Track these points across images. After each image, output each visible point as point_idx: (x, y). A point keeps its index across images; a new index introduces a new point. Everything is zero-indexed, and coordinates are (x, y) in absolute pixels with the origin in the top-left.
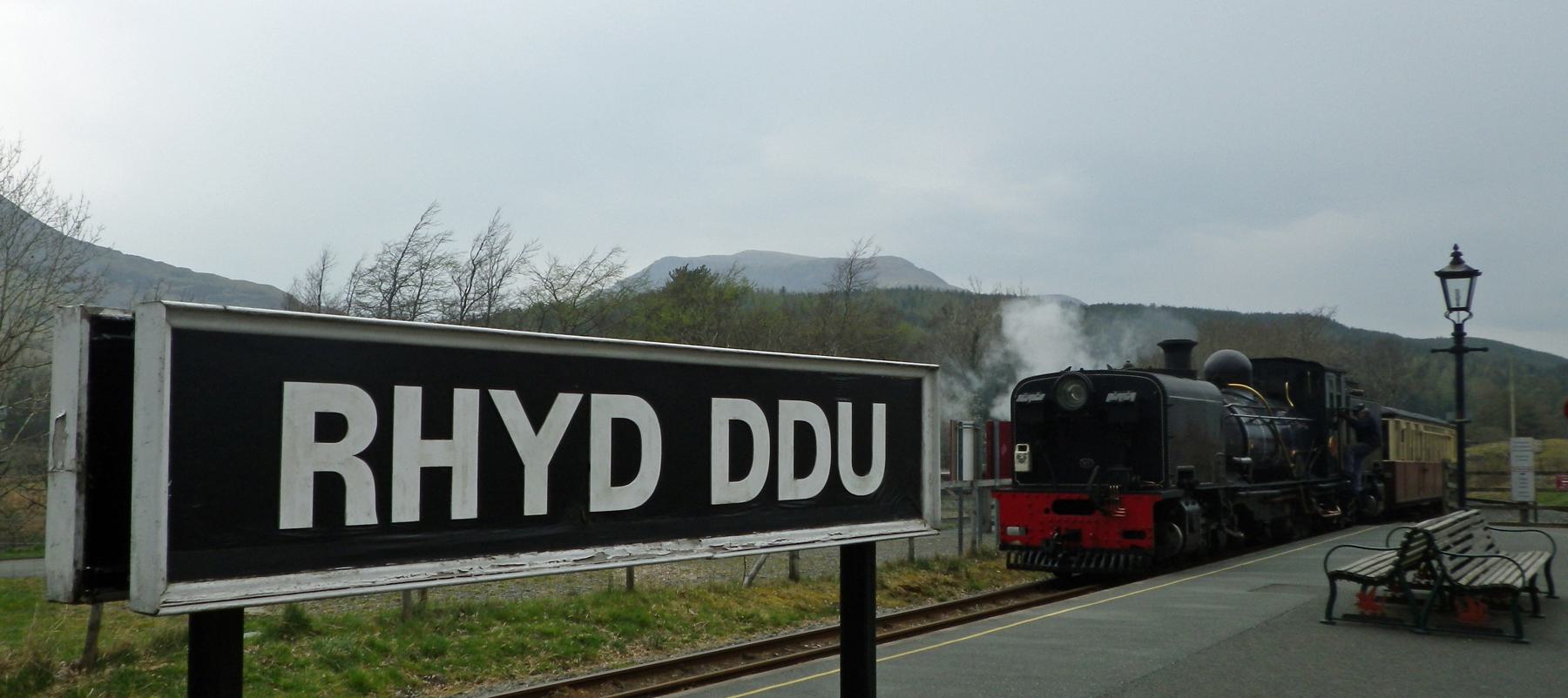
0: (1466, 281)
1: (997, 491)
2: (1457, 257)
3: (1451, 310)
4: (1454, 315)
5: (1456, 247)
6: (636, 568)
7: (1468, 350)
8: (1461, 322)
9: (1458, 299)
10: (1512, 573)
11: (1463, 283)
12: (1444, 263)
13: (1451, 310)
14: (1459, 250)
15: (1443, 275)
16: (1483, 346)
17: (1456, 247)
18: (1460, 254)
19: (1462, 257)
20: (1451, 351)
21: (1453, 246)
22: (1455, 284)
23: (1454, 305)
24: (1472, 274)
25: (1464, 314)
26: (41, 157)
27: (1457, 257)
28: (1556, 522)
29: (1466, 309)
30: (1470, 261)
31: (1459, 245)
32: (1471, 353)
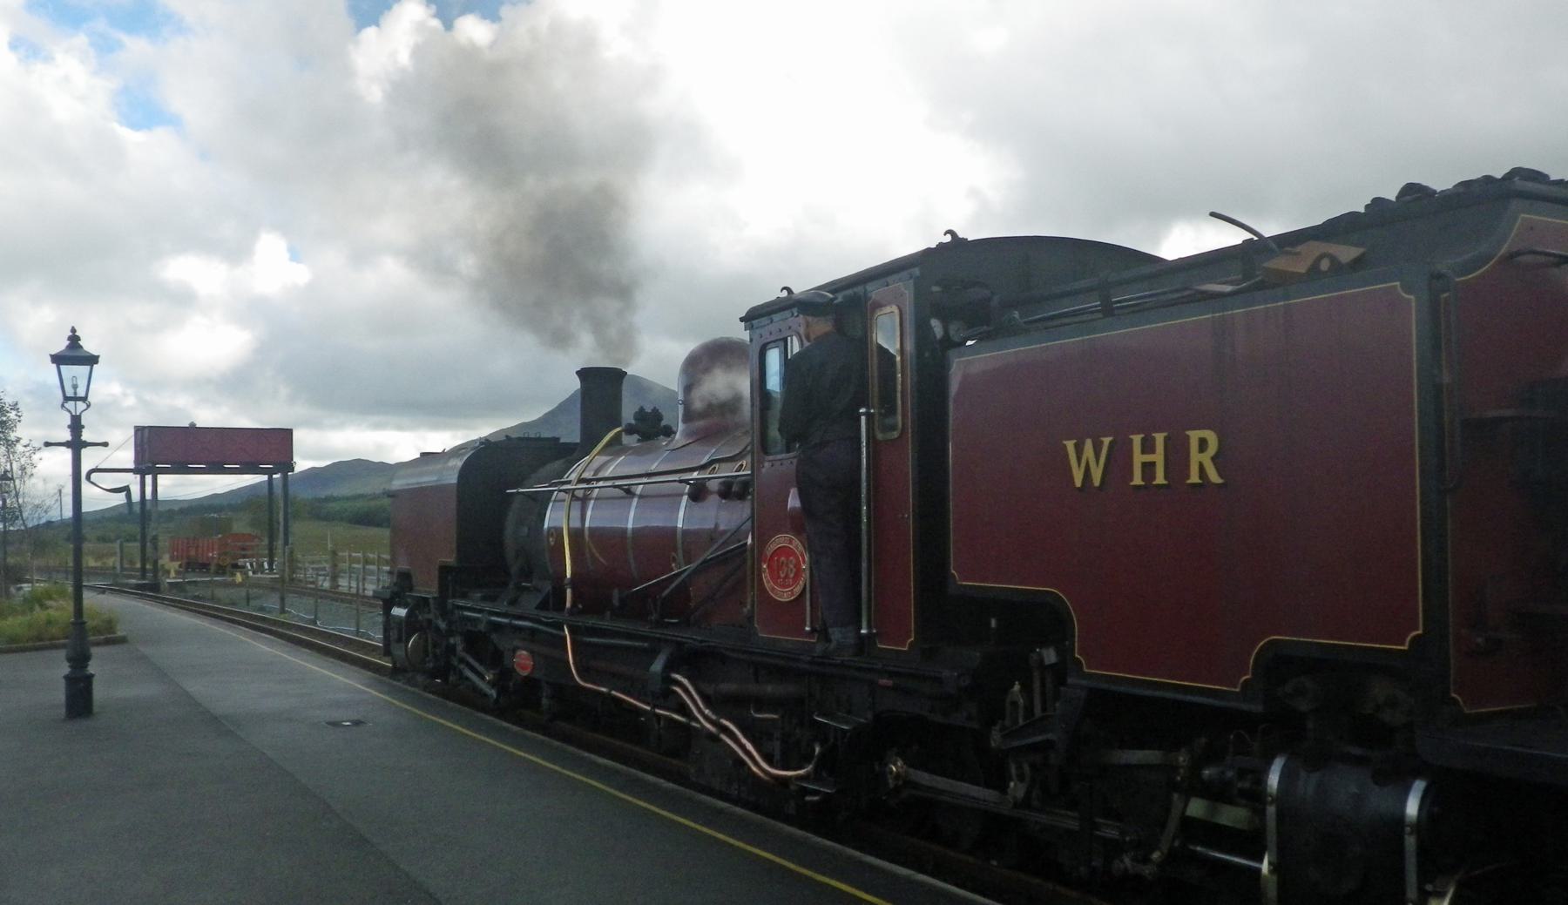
0: (85, 369)
1: (878, 307)
2: (74, 340)
3: (67, 399)
4: (70, 405)
5: (73, 330)
6: (571, 526)
7: (66, 444)
8: (78, 414)
9: (75, 387)
10: (1096, 306)
11: (82, 370)
12: (61, 345)
13: (67, 399)
14: (77, 334)
15: (58, 360)
16: (104, 441)
17: (73, 330)
18: (78, 338)
19: (562, 441)
20: (66, 444)
21: (70, 328)
22: (70, 371)
23: (70, 393)
24: (92, 360)
25: (81, 405)
26: (105, 444)
27: (74, 340)
28: (1539, 249)
29: (84, 399)
30: (89, 345)
31: (76, 328)
32: (64, 441)
